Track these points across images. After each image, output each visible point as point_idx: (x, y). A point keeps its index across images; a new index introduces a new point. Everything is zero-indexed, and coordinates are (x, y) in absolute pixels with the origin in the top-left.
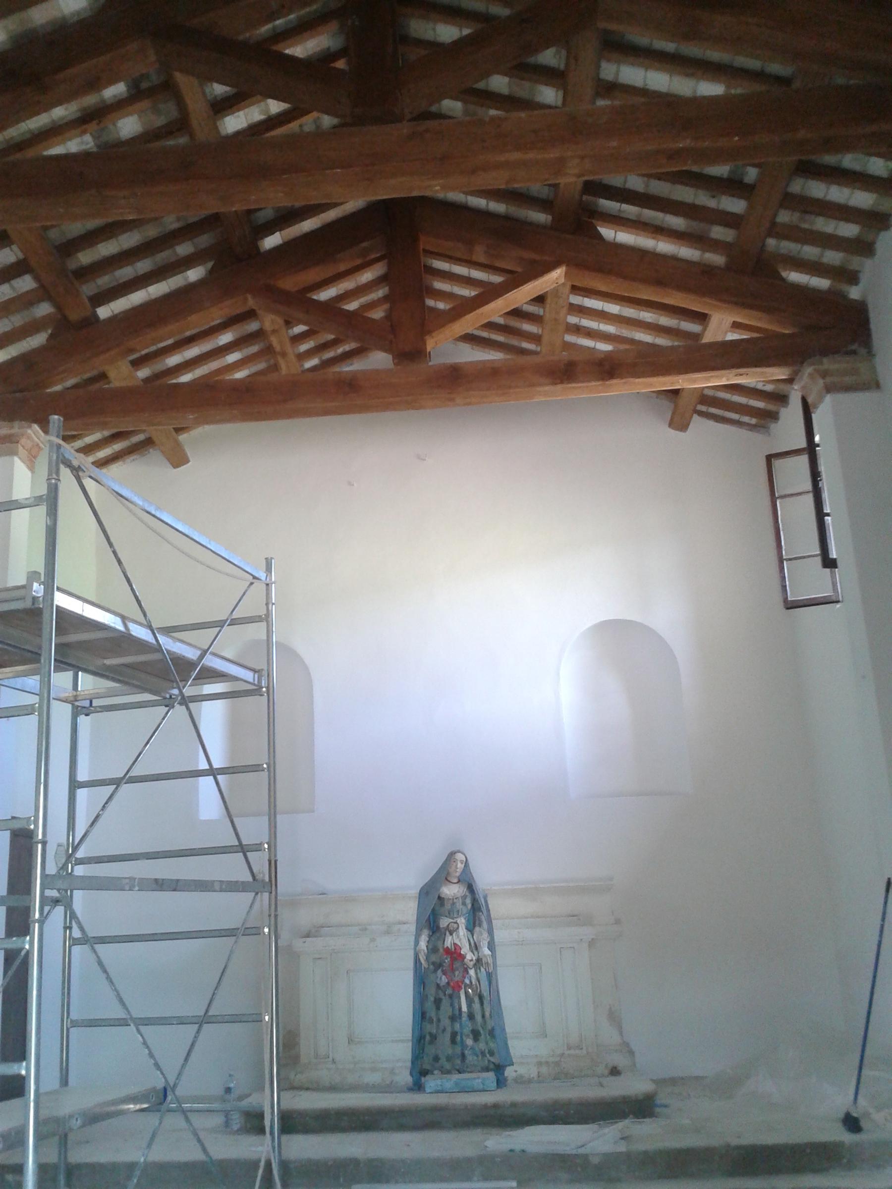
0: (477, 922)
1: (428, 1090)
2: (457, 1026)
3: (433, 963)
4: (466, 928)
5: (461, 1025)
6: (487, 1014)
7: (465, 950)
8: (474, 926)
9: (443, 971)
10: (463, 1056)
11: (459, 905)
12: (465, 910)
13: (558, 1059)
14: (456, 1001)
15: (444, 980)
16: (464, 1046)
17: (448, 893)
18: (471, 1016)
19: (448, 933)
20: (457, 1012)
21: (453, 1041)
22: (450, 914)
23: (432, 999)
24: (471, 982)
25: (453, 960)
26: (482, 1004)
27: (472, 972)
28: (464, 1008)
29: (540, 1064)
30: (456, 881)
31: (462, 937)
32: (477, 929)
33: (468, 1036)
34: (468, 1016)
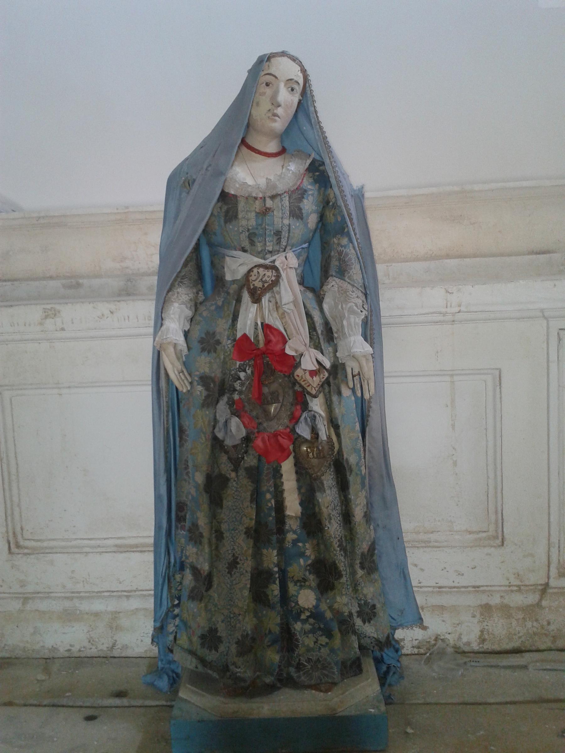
0: (334, 263)
2: (271, 557)
3: (205, 380)
4: (301, 283)
5: (282, 551)
6: (358, 513)
7: (298, 344)
8: (325, 274)
9: (231, 403)
11: (280, 218)
12: (299, 230)
13: (532, 598)
14: (267, 486)
15: (237, 429)
16: (288, 608)
17: (250, 181)
18: (312, 523)
19: (246, 297)
20: (271, 519)
21: (259, 596)
22: (252, 241)
23: (200, 478)
24: (314, 431)
25: (262, 374)
26: (343, 486)
27: (317, 405)
28: (293, 506)
29: (486, 610)
30: (272, 147)
31: (288, 308)
32: (334, 285)
33: (302, 583)
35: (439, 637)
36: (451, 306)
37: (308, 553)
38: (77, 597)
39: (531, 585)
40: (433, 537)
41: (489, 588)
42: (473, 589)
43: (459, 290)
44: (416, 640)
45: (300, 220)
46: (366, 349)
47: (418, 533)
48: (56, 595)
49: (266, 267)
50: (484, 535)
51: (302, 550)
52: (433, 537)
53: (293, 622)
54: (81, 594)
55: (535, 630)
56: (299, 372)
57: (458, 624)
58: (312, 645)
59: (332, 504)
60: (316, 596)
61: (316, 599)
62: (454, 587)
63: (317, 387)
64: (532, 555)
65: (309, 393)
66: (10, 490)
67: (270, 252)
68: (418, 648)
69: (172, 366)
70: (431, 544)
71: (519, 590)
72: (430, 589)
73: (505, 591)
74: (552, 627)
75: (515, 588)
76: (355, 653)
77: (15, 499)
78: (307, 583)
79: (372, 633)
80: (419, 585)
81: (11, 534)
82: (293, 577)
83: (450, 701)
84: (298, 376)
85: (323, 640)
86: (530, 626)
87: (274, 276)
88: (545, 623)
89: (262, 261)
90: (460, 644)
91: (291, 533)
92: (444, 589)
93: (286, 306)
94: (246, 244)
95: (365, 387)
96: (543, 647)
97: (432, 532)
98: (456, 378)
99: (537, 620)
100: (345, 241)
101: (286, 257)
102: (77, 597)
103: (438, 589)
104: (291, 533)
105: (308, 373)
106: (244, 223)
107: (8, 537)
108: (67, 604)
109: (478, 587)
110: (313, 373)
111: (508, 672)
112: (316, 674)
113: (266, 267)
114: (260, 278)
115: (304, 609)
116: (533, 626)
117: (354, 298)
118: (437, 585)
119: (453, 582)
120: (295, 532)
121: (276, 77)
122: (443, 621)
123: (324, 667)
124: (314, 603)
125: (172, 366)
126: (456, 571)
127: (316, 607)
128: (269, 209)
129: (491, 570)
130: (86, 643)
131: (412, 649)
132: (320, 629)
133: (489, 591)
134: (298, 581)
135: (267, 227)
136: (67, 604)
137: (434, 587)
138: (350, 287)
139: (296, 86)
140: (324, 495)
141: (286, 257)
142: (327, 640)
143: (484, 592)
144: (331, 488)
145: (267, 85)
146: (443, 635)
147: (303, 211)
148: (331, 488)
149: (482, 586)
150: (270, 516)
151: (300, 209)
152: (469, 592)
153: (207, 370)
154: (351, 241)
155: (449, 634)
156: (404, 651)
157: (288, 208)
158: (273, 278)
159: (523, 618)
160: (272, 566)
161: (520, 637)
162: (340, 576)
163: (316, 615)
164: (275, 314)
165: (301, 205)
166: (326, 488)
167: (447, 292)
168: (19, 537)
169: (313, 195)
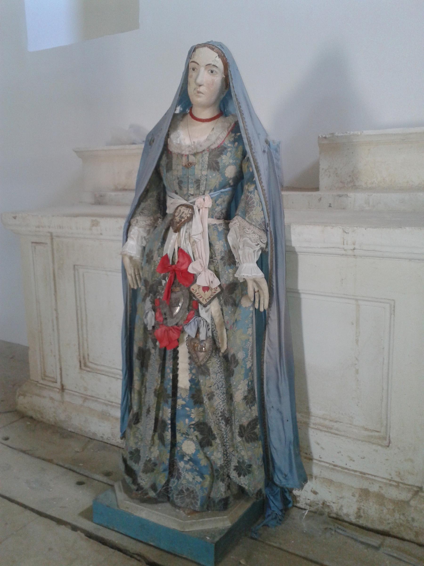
1: (218, 287)
3: (146, 282)
5: (174, 408)
10: (172, 469)
11: (201, 170)
12: (215, 179)
13: (404, 496)
18: (196, 397)
28: (184, 381)
29: (365, 493)
31: (196, 237)
34: (193, 396)
35: (325, 503)
36: (347, 244)
37: (193, 416)
38: (110, 405)
39: (409, 485)
40: (336, 425)
41: (373, 478)
42: (361, 475)
43: (354, 231)
44: (309, 499)
45: (216, 171)
46: (253, 275)
47: (325, 419)
48: (101, 400)
49: (187, 206)
50: (377, 434)
51: (189, 413)
52: (336, 425)
53: (178, 461)
54: (113, 404)
55: (401, 521)
56: (194, 288)
57: (341, 498)
58: (191, 480)
59: (216, 386)
60: (196, 447)
61: (195, 449)
62: (346, 469)
63: (208, 299)
64: (412, 461)
65: (201, 303)
66: (82, 330)
67: (192, 195)
68: (310, 506)
69: (130, 271)
70: (333, 431)
71: (397, 486)
72: (327, 465)
73: (385, 484)
74: (415, 524)
75: (394, 484)
76: (222, 495)
77: (85, 336)
78: (190, 437)
79: (244, 484)
80: (320, 459)
81: (82, 357)
82: (180, 430)
83: (297, 553)
84: (193, 289)
85: (199, 479)
86: (398, 518)
87: (189, 214)
88: (410, 519)
89: (185, 202)
90: (340, 513)
91: (181, 399)
92: (336, 468)
93: (196, 237)
94: (177, 188)
95: (262, 302)
96: (407, 538)
97: (336, 422)
98: (360, 302)
99: (404, 514)
100: (252, 188)
101: (204, 199)
102: (110, 405)
103: (333, 467)
104: (181, 399)
105: (201, 289)
106: (175, 173)
107: (80, 358)
108: (105, 408)
109: (364, 474)
110: (206, 289)
111: (361, 547)
112: (188, 500)
113: (187, 206)
114: (180, 214)
115: (186, 454)
116: (400, 518)
117: (249, 234)
118: (333, 463)
119: (346, 464)
120: (184, 399)
121: (198, 64)
122: (330, 492)
123: (194, 498)
124: (194, 452)
125: (130, 271)
126: (349, 457)
127: (194, 455)
128: (191, 164)
129: (379, 465)
130: (110, 436)
131: (306, 505)
132: (196, 470)
133: (373, 479)
134: (183, 433)
135: (189, 176)
136: (105, 408)
137: (330, 464)
138: (247, 225)
139: (214, 69)
140: (208, 378)
141: (204, 199)
142: (201, 480)
143: (367, 479)
144: (217, 374)
145: (194, 69)
146: (329, 503)
147: (220, 164)
148: (217, 374)
149: (368, 474)
150: (169, 385)
151: (217, 163)
152: (356, 476)
153: (147, 277)
154: (256, 188)
155: (334, 503)
156: (298, 505)
157: (207, 163)
158: (189, 215)
159: (393, 510)
160: (167, 419)
161: (389, 524)
162: (215, 438)
163: (193, 460)
164: (188, 242)
165: (219, 160)
166: (211, 373)
167: (344, 232)
168: (87, 360)
169: (230, 151)
